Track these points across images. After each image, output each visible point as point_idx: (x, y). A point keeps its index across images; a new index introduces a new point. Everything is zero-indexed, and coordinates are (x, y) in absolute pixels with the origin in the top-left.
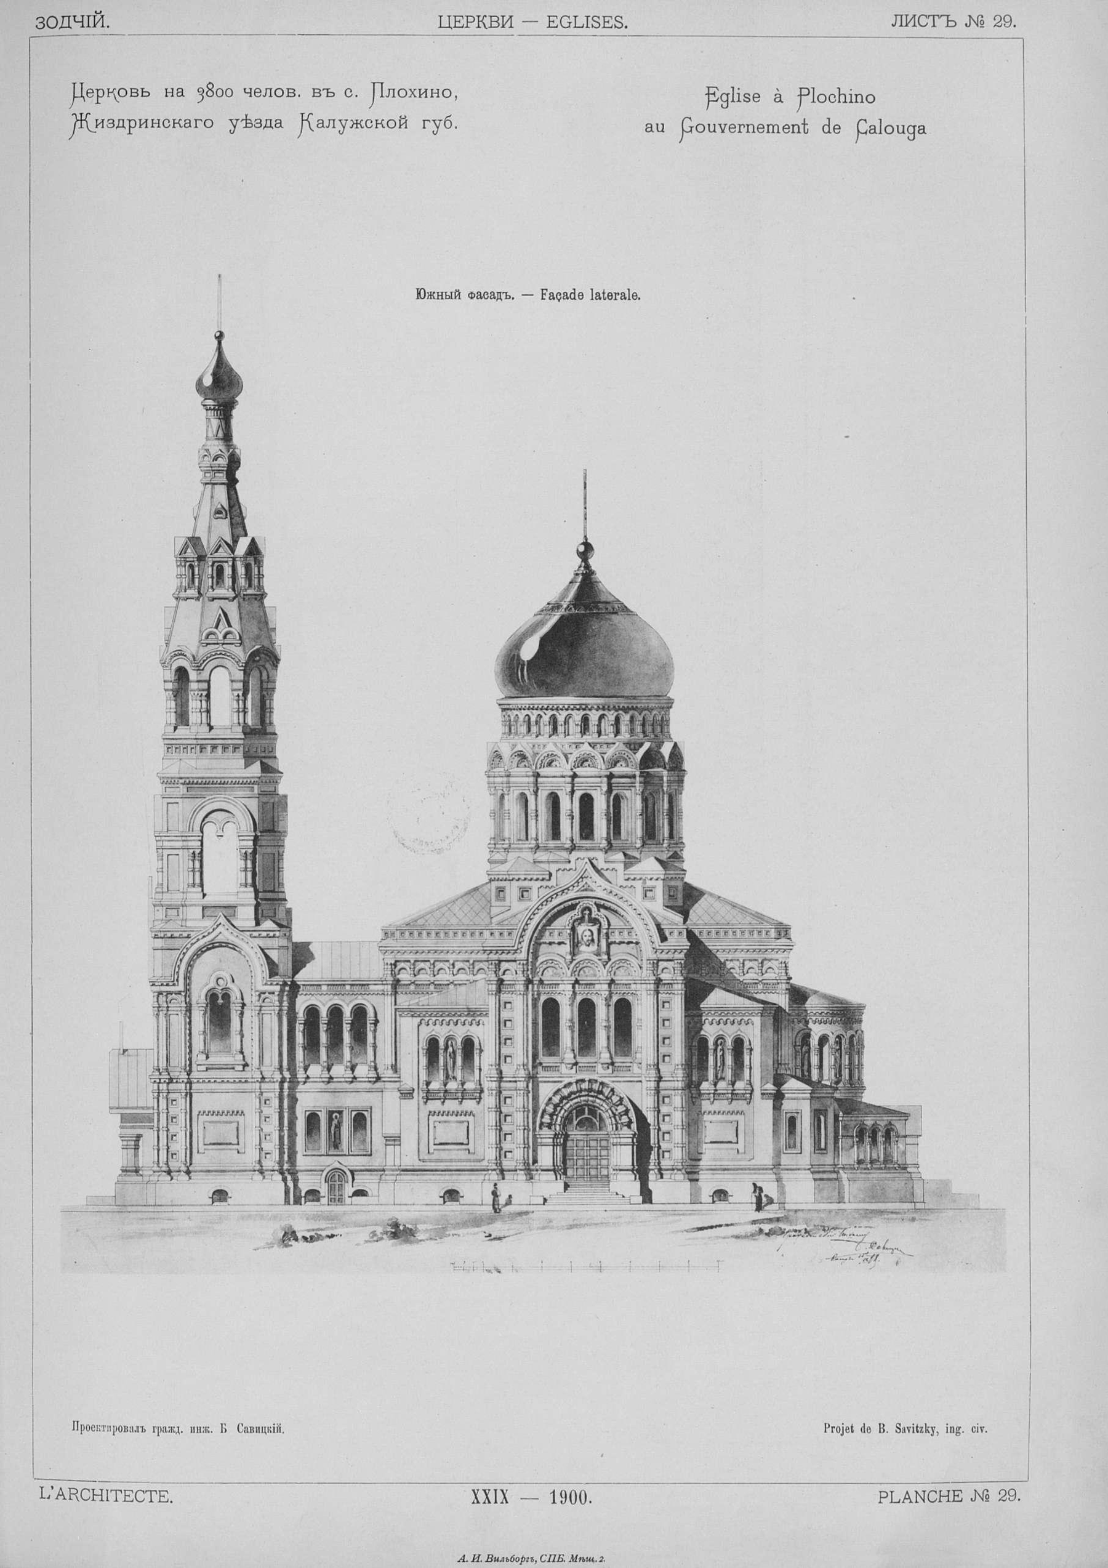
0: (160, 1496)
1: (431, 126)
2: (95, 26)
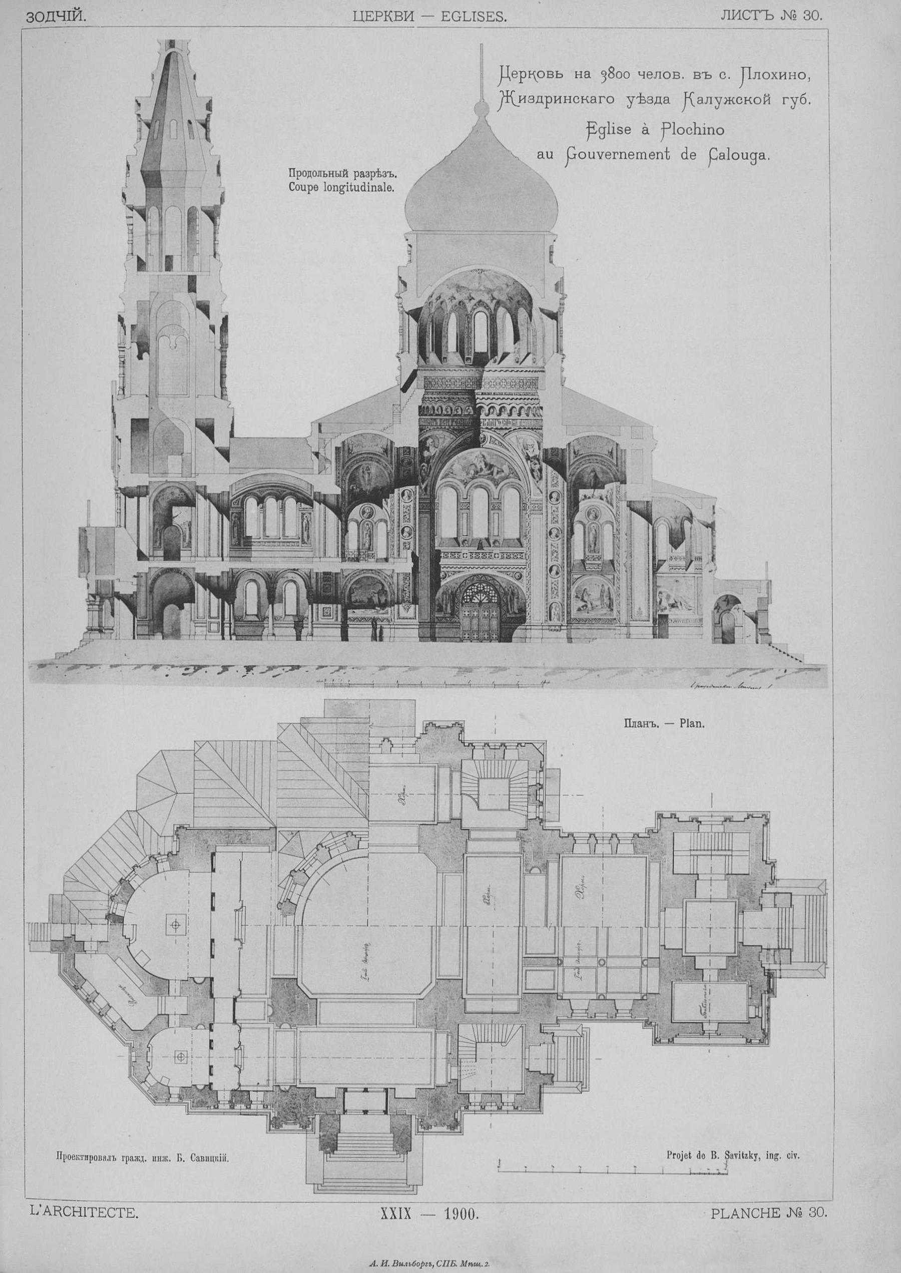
0: (129, 1213)
1: (789, 102)
2: (74, 20)
